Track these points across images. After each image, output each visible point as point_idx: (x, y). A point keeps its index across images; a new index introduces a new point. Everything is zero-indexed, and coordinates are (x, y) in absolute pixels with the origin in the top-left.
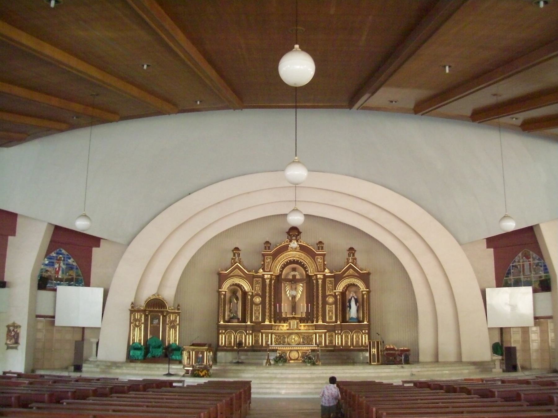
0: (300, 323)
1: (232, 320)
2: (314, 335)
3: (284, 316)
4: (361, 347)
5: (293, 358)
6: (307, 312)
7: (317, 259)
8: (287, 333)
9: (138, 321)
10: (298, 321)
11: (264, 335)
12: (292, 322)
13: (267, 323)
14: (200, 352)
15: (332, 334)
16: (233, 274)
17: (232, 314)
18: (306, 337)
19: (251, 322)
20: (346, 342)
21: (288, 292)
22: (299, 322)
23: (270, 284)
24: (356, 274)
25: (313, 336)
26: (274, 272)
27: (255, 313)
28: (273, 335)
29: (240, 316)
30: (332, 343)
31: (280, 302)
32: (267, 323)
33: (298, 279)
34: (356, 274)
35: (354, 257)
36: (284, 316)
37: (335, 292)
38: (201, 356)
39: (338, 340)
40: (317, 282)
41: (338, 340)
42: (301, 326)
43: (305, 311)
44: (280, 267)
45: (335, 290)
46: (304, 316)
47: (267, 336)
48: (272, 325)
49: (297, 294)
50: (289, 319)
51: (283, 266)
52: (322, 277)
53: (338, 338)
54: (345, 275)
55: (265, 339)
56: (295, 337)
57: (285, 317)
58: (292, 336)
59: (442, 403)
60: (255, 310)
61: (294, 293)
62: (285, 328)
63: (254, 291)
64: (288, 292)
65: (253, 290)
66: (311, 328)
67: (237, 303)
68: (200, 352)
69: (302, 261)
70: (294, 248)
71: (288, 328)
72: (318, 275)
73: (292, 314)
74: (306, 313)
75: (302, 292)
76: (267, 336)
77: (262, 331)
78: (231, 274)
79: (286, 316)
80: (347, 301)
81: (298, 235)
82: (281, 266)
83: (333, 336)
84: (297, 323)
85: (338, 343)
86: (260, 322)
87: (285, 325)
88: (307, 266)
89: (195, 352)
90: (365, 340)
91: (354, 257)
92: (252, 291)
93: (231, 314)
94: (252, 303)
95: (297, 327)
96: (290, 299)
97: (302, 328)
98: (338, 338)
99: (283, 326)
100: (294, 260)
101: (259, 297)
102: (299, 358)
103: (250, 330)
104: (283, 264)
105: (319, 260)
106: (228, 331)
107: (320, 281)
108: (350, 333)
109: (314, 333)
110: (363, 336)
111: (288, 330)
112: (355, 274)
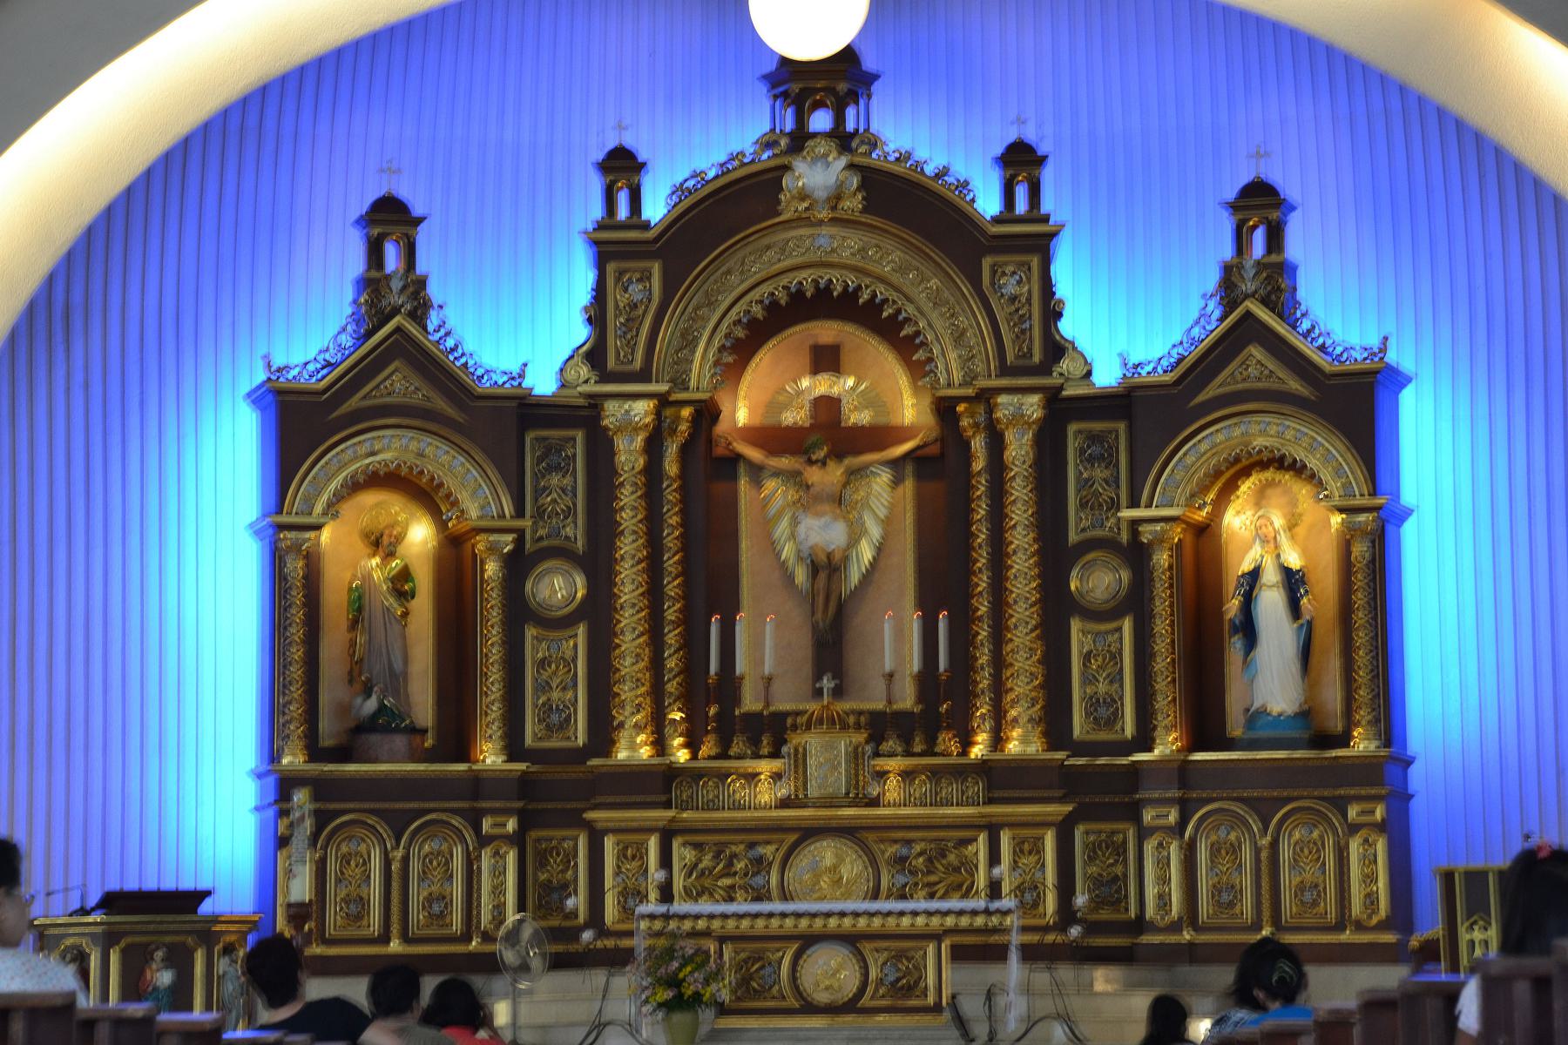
0: (877, 754)
1: (374, 738)
2: (982, 838)
3: (750, 702)
4: (1339, 927)
5: (822, 998)
6: (927, 678)
7: (994, 273)
8: (779, 828)
9: (714, 455)
10: (859, 737)
11: (609, 843)
12: (813, 742)
13: (634, 749)
14: (159, 955)
15: (1113, 833)
16: (364, 397)
17: (369, 696)
18: (920, 854)
19: (514, 747)
20: (1226, 895)
21: (784, 524)
22: (869, 749)
23: (653, 471)
24: (1295, 385)
25: (971, 848)
26: (672, 381)
27: (543, 687)
28: (676, 844)
29: (423, 704)
30: (1119, 901)
31: (727, 604)
32: (634, 749)
33: (858, 430)
34: (1295, 385)
35: (1274, 258)
36: (750, 702)
37: (1135, 523)
38: (165, 978)
39: (1164, 880)
40: (996, 443)
41: (1164, 880)
42: (881, 775)
43: (916, 665)
44: (716, 343)
45: (1134, 503)
46: (907, 699)
47: (632, 853)
48: (672, 774)
49: (853, 542)
50: (795, 727)
51: (783, 298)
52: (1032, 406)
53: (1163, 864)
54: (1201, 398)
55: (617, 873)
56: (840, 860)
57: (759, 715)
58: (546, 580)
59: (1160, 896)
60: (542, 664)
61: (824, 532)
62: (766, 794)
63: (526, 523)
64: (784, 524)
65: (520, 512)
66: (951, 789)
67: (405, 614)
68: (159, 955)
69: (882, 291)
70: (821, 194)
71: (783, 792)
72: (1002, 399)
73: (818, 693)
74: (735, 607)
75: (887, 523)
76: (632, 853)
77: (591, 815)
78: (354, 402)
79: (767, 704)
80: (1230, 583)
81: (853, 96)
82: (727, 336)
83: (1121, 849)
84: (855, 756)
85: (1163, 901)
86: (576, 750)
87: (765, 767)
88: (918, 333)
89: (125, 953)
90: (1370, 878)
91: (1274, 258)
92: (518, 523)
93: (359, 700)
94: (519, 611)
95: (854, 780)
96: (801, 576)
97: (892, 788)
98: (1163, 864)
99: (752, 777)
100: (824, 292)
101: (566, 566)
102: (870, 990)
103: (507, 812)
104: (738, 322)
105: (1010, 286)
106: (338, 821)
107: (1019, 448)
108: (1249, 828)
109: (980, 828)
110: (1355, 846)
111: (784, 803)
112: (1283, 387)
